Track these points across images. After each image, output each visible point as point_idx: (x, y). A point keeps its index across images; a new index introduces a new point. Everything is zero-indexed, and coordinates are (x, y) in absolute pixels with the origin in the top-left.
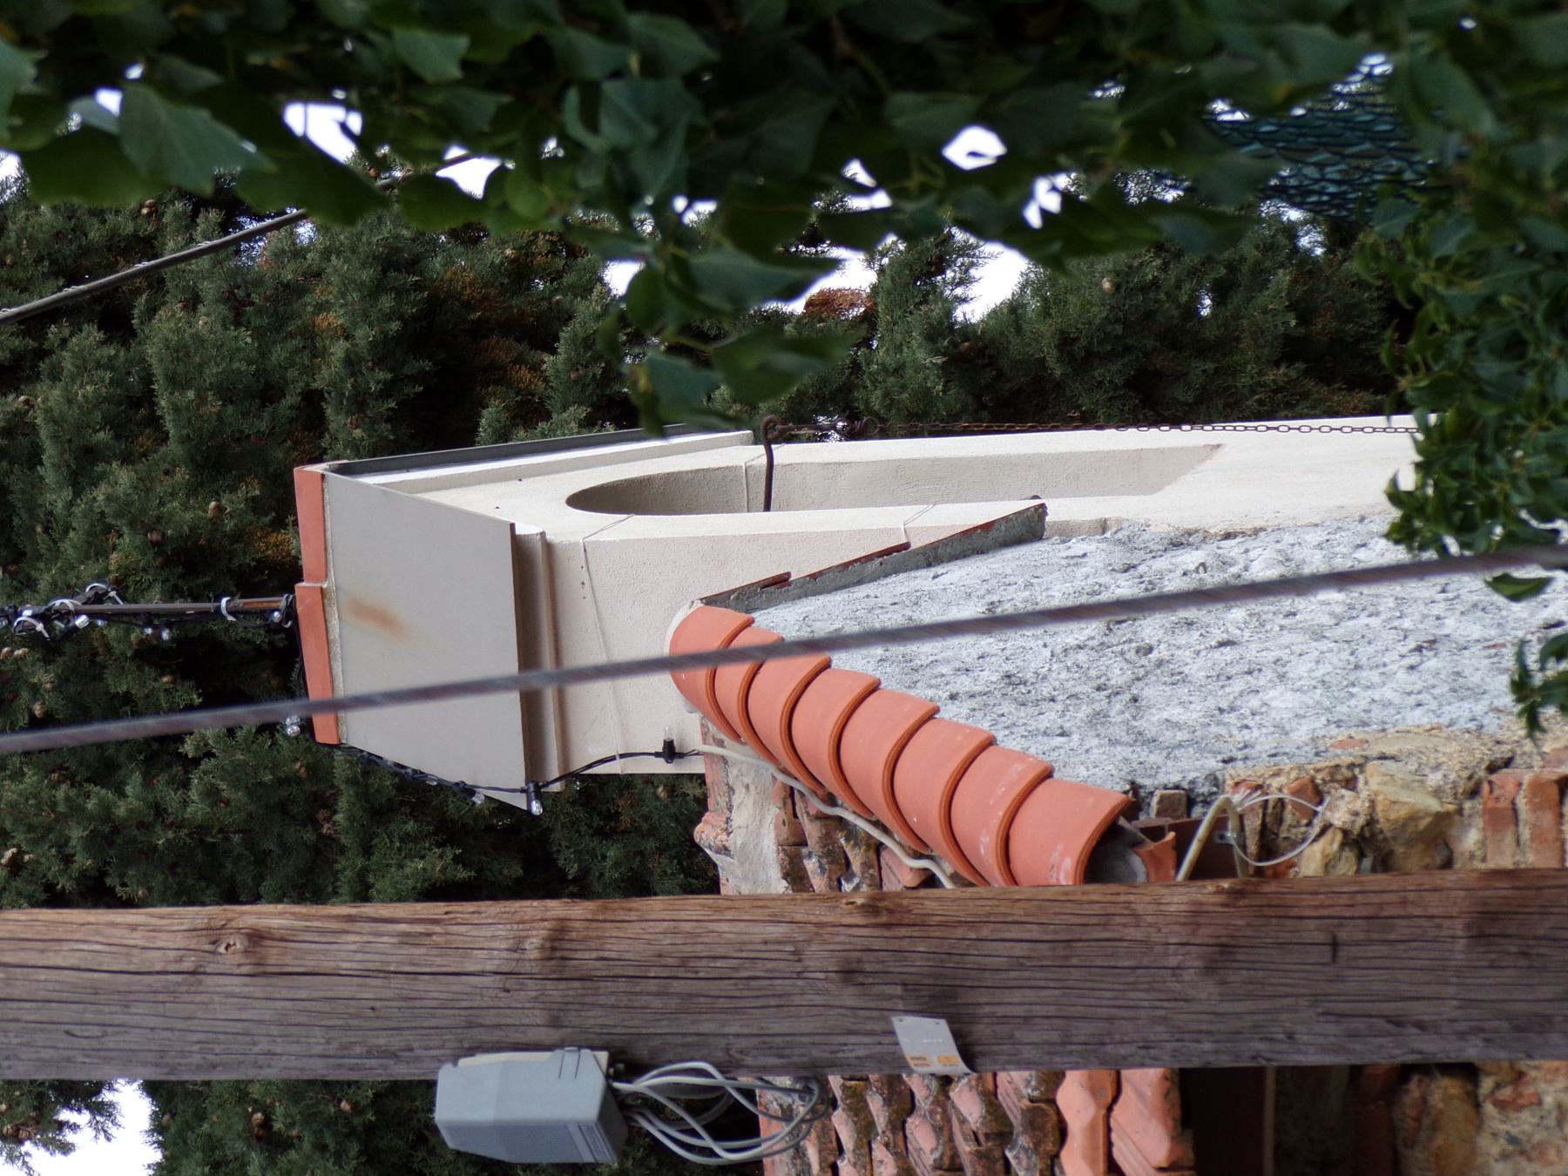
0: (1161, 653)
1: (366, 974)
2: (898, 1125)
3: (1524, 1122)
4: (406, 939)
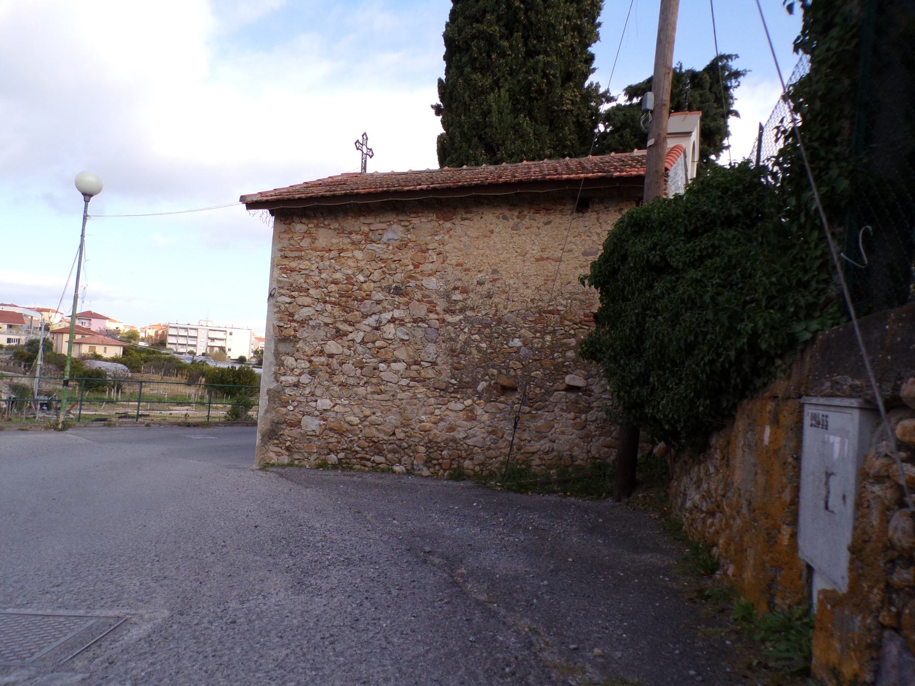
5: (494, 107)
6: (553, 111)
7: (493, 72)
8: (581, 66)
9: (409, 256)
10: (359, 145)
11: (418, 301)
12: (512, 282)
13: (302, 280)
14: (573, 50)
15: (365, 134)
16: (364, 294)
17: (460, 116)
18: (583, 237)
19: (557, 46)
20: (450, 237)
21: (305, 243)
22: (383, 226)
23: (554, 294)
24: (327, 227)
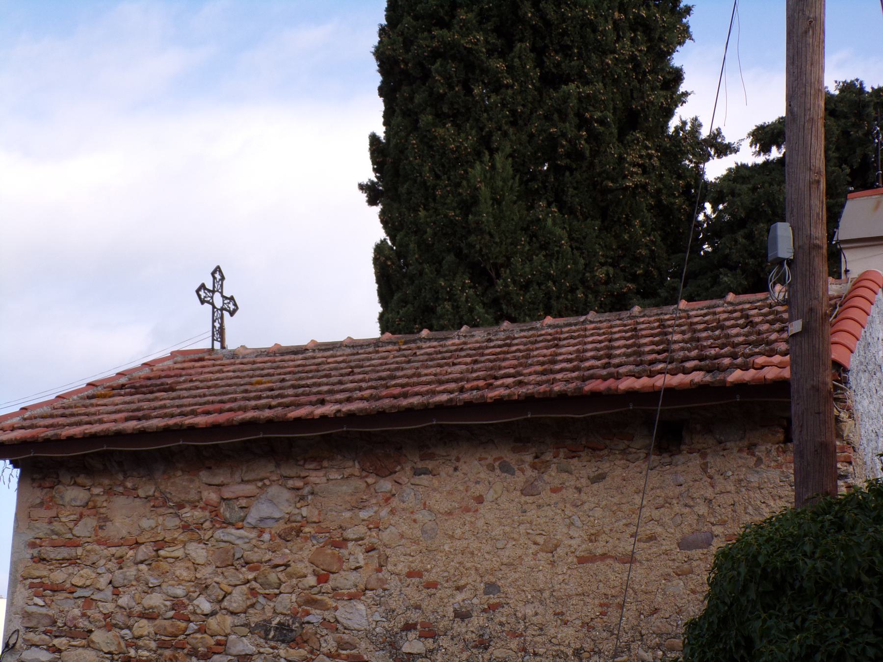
0: (875, 377)
1: (810, 206)
2: (767, 322)
3: (774, 453)
4: (818, 215)
5: (484, 191)
6: (606, 191)
7: (477, 120)
8: (656, 97)
9: (306, 554)
10: (203, 294)
11: (329, 655)
12: (529, 611)
13: (77, 612)
14: (637, 66)
15: (218, 269)
16: (211, 642)
17: (416, 211)
18: (677, 508)
19: (602, 62)
20: (392, 512)
21: (84, 529)
22: (249, 489)
23: (625, 638)
24: (131, 493)
